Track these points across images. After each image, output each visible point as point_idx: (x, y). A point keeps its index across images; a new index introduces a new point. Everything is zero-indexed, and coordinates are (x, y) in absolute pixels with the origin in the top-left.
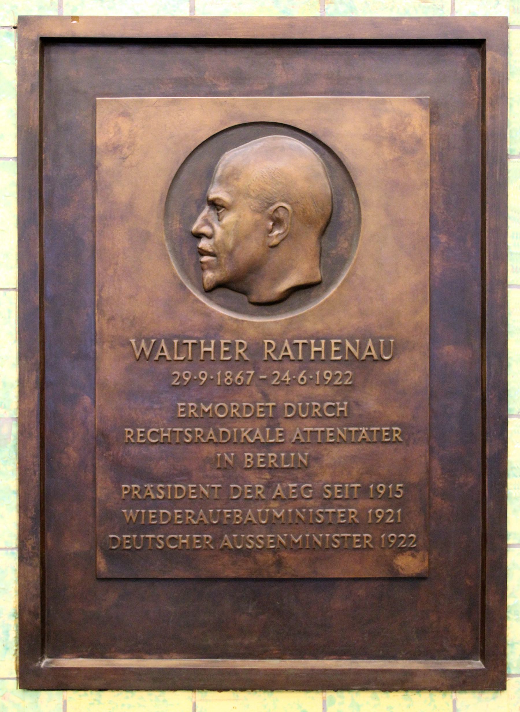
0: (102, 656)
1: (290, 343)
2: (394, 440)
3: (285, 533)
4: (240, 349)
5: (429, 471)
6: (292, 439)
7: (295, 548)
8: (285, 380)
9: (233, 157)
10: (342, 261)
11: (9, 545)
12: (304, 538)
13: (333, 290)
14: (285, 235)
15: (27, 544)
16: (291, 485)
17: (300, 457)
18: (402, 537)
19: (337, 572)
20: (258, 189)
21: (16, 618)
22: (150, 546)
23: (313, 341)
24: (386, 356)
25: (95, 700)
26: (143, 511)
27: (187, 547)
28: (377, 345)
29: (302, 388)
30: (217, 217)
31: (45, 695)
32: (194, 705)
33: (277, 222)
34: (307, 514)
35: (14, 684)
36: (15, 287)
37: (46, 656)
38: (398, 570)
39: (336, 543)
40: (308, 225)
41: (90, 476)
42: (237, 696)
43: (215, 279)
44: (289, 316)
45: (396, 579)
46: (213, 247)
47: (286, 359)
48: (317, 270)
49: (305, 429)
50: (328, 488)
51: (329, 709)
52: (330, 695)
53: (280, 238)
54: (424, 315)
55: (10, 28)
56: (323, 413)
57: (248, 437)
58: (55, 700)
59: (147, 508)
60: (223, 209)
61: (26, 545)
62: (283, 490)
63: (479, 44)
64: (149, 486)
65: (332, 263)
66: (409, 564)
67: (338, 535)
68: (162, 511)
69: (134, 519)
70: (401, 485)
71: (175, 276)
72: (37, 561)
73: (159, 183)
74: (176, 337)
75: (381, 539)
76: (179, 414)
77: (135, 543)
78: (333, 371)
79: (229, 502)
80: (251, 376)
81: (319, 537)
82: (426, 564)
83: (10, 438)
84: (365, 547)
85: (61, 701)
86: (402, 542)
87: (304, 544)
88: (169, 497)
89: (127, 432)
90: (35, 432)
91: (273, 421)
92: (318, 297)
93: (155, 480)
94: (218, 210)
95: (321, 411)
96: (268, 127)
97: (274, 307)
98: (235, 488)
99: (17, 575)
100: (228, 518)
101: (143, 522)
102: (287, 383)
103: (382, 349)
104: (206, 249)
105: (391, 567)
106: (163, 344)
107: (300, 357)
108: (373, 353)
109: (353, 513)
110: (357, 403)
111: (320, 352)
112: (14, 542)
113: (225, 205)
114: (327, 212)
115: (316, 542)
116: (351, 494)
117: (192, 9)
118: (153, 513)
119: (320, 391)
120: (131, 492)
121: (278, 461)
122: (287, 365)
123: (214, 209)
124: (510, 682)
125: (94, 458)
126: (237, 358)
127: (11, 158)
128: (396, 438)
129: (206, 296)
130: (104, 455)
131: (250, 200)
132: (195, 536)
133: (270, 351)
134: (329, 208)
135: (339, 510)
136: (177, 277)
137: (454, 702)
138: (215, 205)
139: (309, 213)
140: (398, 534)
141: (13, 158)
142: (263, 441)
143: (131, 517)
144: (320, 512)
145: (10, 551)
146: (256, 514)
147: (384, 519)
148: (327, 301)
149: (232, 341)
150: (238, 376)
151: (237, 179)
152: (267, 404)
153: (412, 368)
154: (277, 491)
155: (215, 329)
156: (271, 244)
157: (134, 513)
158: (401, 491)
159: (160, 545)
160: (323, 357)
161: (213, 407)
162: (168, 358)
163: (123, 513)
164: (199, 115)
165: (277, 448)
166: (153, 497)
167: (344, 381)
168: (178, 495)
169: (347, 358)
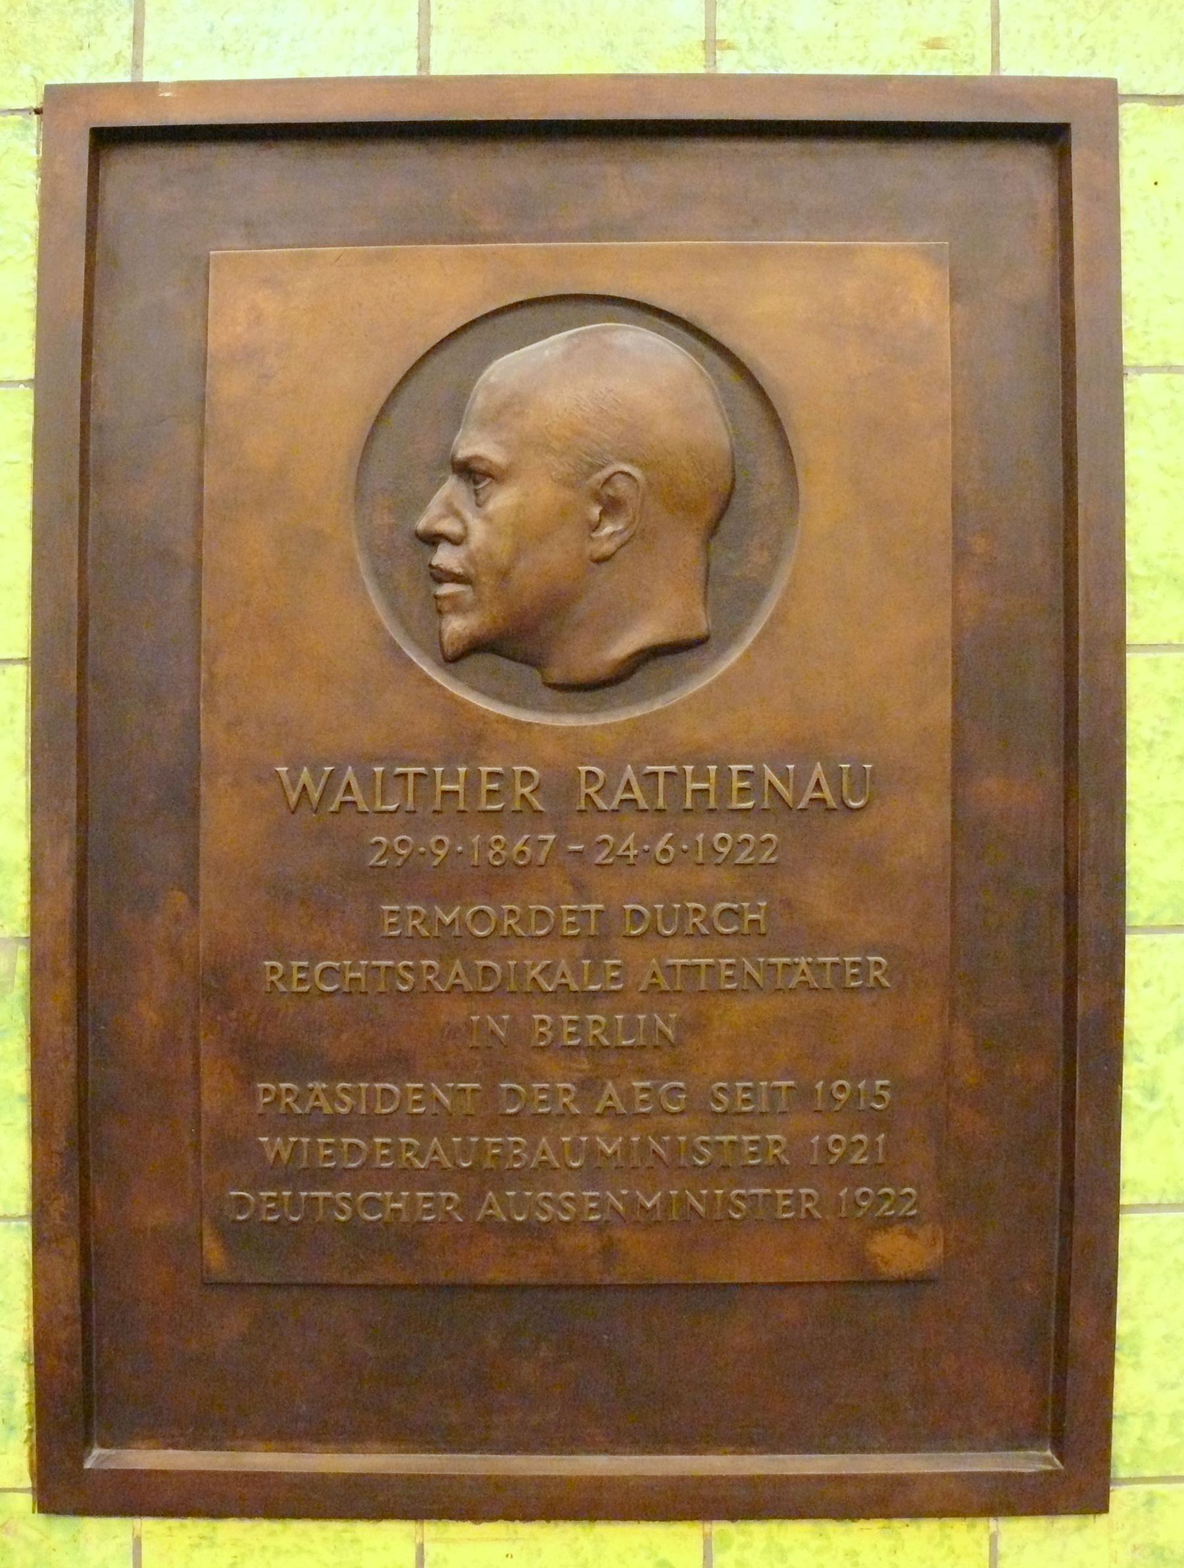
0: (217, 1444)
1: (636, 773)
2: (872, 983)
3: (624, 1188)
4: (523, 785)
5: (947, 1049)
6: (639, 984)
7: (648, 1221)
8: (627, 853)
9: (507, 370)
10: (753, 593)
11: (13, 1211)
12: (666, 1198)
13: (734, 655)
14: (626, 535)
15: (51, 1210)
16: (637, 1084)
17: (660, 1022)
18: (887, 1195)
19: (736, 1270)
20: (568, 434)
21: (29, 1365)
22: (320, 1216)
23: (689, 768)
24: (854, 800)
25: (203, 1538)
26: (305, 1140)
27: (404, 1218)
28: (835, 776)
29: (667, 870)
30: (474, 497)
31: (92, 1526)
32: (420, 1550)
33: (612, 506)
34: (674, 1148)
35: (24, 1502)
36: (24, 655)
37: (96, 1444)
38: (876, 1266)
39: (738, 1209)
40: (680, 514)
41: (188, 1062)
42: (516, 1532)
43: (468, 631)
44: (637, 712)
45: (871, 1281)
46: (466, 564)
47: (626, 808)
48: (699, 611)
49: (671, 962)
50: (721, 1089)
51: (719, 1559)
52: (721, 1529)
53: (618, 540)
54: (941, 708)
55: (27, 113)
56: (711, 927)
57: (541, 980)
58: (115, 1537)
59: (314, 1133)
60: (488, 480)
61: (47, 1212)
62: (621, 1096)
63: (1052, 137)
64: (319, 1086)
65: (731, 595)
66: (900, 1252)
67: (743, 1192)
68: (346, 1140)
69: (285, 1156)
70: (886, 1082)
71: (378, 628)
72: (72, 1246)
73: (345, 428)
74: (379, 760)
75: (839, 1198)
76: (386, 929)
77: (286, 1210)
78: (735, 832)
79: (498, 1122)
80: (547, 848)
81: (701, 1195)
82: (939, 1249)
83: (13, 982)
84: (803, 1215)
85: (129, 1539)
86: (886, 1205)
87: (666, 1210)
88: (363, 1111)
89: (268, 969)
90: (67, 968)
91: (599, 942)
92: (697, 670)
93: (331, 1072)
94: (476, 483)
95: (708, 921)
96: (591, 308)
97: (599, 694)
98: (511, 1091)
99: (30, 1274)
100: (494, 1156)
101: (304, 1165)
102: (631, 860)
103: (845, 786)
104: (448, 568)
105: (860, 1259)
106: (350, 774)
107: (661, 803)
108: (827, 794)
109: (777, 1143)
110: (788, 904)
111: (707, 790)
112: (21, 1202)
113: (494, 473)
114: (722, 485)
115: (692, 1208)
116: (772, 1103)
117: (424, 62)
118: (327, 1145)
119: (707, 877)
120: (278, 1098)
121: (609, 1031)
122: (629, 819)
123: (467, 481)
124: (1118, 1496)
125: (195, 1026)
126: (517, 806)
127: (21, 382)
128: (876, 979)
129: (449, 672)
130: (219, 1018)
131: (550, 458)
132: (420, 1194)
133: (591, 791)
134: (728, 476)
135: (746, 1138)
136: (383, 629)
137: (993, 1539)
138: (471, 472)
139: (682, 487)
140: (877, 1187)
141: (27, 383)
142: (574, 987)
143: (278, 1153)
144: (704, 1143)
145: (13, 1224)
146: (559, 1149)
147: (846, 1156)
148: (722, 680)
149: (505, 769)
150: (519, 846)
151: (520, 414)
152: (585, 907)
153: (916, 826)
154: (605, 1096)
155: (470, 738)
156: (596, 556)
157: (286, 1143)
158: (886, 1094)
159: (342, 1212)
160: (712, 804)
161: (460, 914)
162: (363, 807)
163: (260, 1144)
164: (442, 285)
165: (605, 1004)
166: (327, 1110)
167: (759, 857)
168: (383, 1106)
169: (766, 805)
